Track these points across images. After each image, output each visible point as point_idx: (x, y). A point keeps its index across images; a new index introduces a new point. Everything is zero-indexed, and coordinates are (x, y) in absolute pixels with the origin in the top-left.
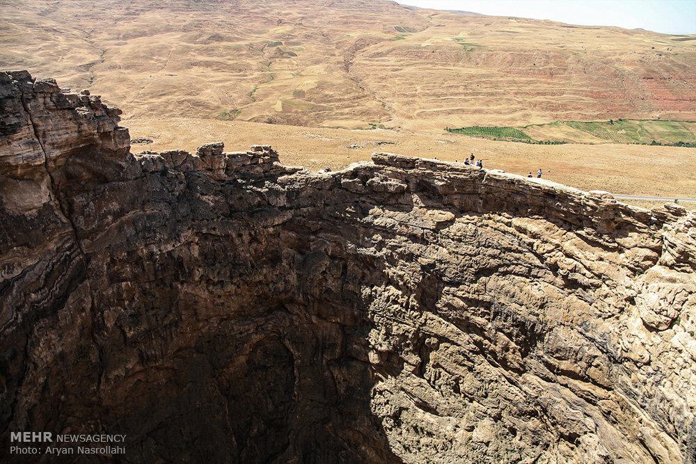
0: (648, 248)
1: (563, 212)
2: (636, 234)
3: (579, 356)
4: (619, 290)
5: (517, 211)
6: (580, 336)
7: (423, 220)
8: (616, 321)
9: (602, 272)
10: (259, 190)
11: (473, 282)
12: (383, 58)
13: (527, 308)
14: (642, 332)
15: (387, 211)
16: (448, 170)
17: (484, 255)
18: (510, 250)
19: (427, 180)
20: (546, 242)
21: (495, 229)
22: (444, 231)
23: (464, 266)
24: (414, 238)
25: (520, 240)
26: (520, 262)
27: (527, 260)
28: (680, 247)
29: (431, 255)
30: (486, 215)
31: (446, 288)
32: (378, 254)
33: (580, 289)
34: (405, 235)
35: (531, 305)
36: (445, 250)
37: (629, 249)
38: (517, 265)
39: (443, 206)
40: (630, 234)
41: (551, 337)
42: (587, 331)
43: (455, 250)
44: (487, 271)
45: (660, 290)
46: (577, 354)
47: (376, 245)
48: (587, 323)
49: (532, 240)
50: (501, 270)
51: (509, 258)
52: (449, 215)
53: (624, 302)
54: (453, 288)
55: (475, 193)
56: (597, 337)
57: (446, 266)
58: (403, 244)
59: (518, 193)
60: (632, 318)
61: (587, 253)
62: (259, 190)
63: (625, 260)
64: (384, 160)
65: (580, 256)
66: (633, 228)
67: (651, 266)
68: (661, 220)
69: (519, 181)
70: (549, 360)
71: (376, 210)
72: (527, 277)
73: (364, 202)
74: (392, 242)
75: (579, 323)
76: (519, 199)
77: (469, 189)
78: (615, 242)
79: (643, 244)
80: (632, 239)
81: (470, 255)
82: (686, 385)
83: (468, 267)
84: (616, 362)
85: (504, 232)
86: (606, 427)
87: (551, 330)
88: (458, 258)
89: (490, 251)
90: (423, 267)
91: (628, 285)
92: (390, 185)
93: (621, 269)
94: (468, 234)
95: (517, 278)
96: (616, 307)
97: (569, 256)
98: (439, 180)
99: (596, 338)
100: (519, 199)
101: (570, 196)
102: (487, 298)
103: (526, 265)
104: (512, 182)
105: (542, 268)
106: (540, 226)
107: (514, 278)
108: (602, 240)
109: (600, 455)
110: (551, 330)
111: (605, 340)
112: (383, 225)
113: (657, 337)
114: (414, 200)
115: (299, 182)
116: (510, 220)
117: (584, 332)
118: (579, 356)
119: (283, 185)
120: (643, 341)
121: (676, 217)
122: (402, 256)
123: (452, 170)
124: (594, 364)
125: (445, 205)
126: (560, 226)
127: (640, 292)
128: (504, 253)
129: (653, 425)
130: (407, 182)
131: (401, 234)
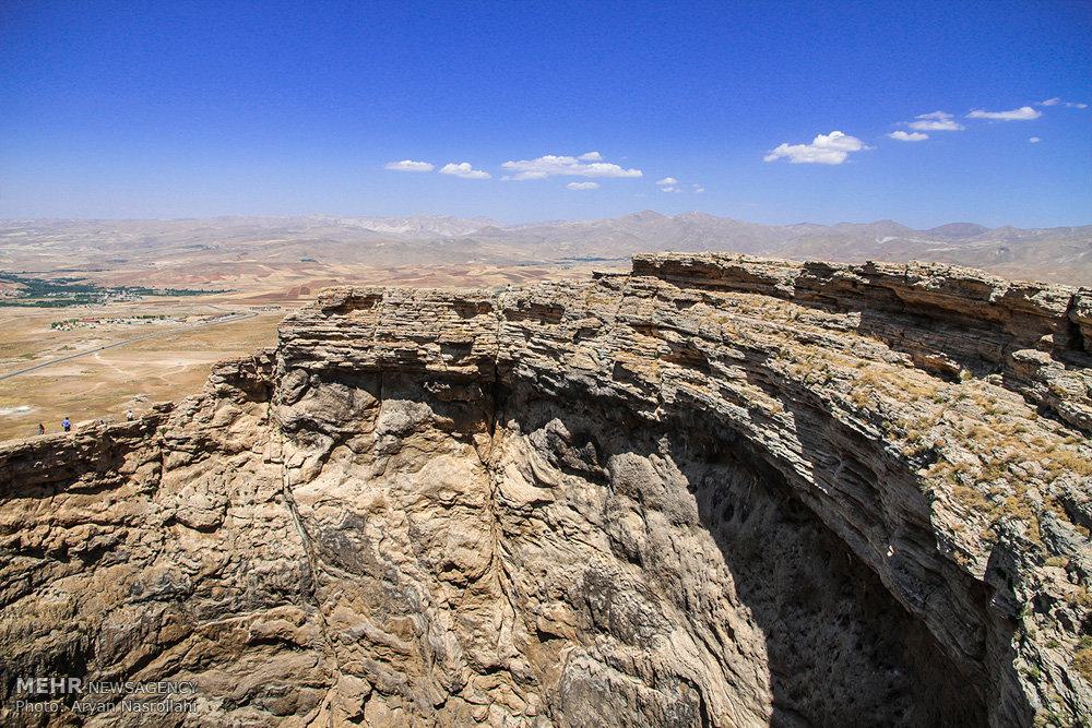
0: (147, 462)
1: (46, 471)
4: (151, 521)
6: (135, 606)
20: (34, 526)
27: (20, 568)
28: (195, 438)
37: (134, 473)
49: (13, 537)
56: (157, 589)
61: (94, 506)
63: (136, 487)
65: (87, 514)
66: (126, 448)
67: (160, 478)
68: (153, 424)
70: (110, 673)
72: (30, 592)
75: (127, 592)
80: (131, 461)
82: (276, 545)
86: (203, 678)
91: (155, 510)
95: (16, 605)
99: (157, 589)
105: (45, 564)
106: (16, 510)
107: (13, 608)
108: (106, 480)
109: (219, 710)
113: (223, 531)
117: (137, 598)
120: (212, 546)
126: (41, 496)
127: (177, 506)
129: (258, 614)
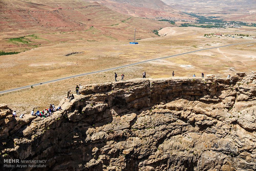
2: (224, 91)
3: (216, 163)
4: (227, 120)
5: (167, 100)
6: (214, 152)
7: (121, 124)
8: (229, 136)
9: (217, 114)
10: (12, 150)
11: (156, 150)
12: (233, 17)
13: (188, 151)
14: (247, 134)
15: (97, 128)
16: (132, 85)
17: (159, 131)
18: (170, 122)
19: (120, 96)
20: (186, 110)
21: (160, 113)
22: (134, 126)
23: (150, 143)
24: (117, 139)
25: (173, 114)
26: (176, 127)
29: (130, 145)
30: (153, 108)
31: (140, 163)
32: (97, 162)
33: (208, 128)
34: (112, 140)
35: (189, 148)
36: (137, 138)
38: (174, 129)
39: (128, 110)
40: (222, 92)
41: (200, 161)
42: (217, 148)
43: (144, 135)
44: (161, 141)
45: (248, 112)
46: (215, 163)
47: (95, 156)
48: (216, 144)
49: (179, 112)
50: (168, 135)
51: (170, 127)
52: (133, 115)
53: (230, 125)
54: (144, 161)
55: (147, 95)
56: (224, 148)
57: (140, 148)
58: (112, 146)
59: (167, 88)
60: (238, 131)
61: (207, 108)
62: (12, 150)
63: (224, 105)
64: (91, 90)
65: (204, 111)
66: (223, 88)
68: (235, 80)
69: (170, 81)
71: (90, 130)
72: (181, 134)
73: (81, 127)
74: (105, 149)
75: (212, 145)
76: (168, 91)
77: (143, 94)
78: (218, 98)
79: (229, 95)
80: (224, 94)
81: (152, 135)
83: (152, 143)
84: (236, 155)
85: (164, 113)
87: (200, 156)
88: (146, 140)
89: (161, 127)
90: (127, 156)
92: (99, 107)
93: (224, 110)
94: (148, 122)
95: (176, 137)
96: (228, 129)
97: (197, 113)
98: (127, 93)
100: (168, 91)
101: (198, 81)
102: (165, 156)
103: (179, 127)
104: (166, 82)
106: (181, 102)
110: (200, 156)
111: (229, 147)
112: (98, 138)
114: (112, 112)
115: (40, 128)
116: (165, 105)
117: (216, 149)
118: (216, 163)
119: (29, 137)
120: (250, 138)
121: (242, 77)
122: (112, 155)
123: (135, 84)
124: (224, 163)
125: (129, 109)
127: (239, 117)
128: (168, 125)
130: (106, 101)
131: (109, 140)
